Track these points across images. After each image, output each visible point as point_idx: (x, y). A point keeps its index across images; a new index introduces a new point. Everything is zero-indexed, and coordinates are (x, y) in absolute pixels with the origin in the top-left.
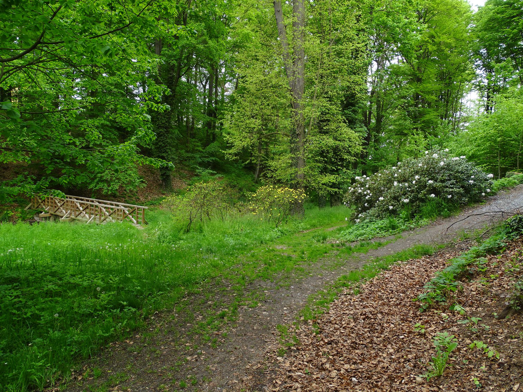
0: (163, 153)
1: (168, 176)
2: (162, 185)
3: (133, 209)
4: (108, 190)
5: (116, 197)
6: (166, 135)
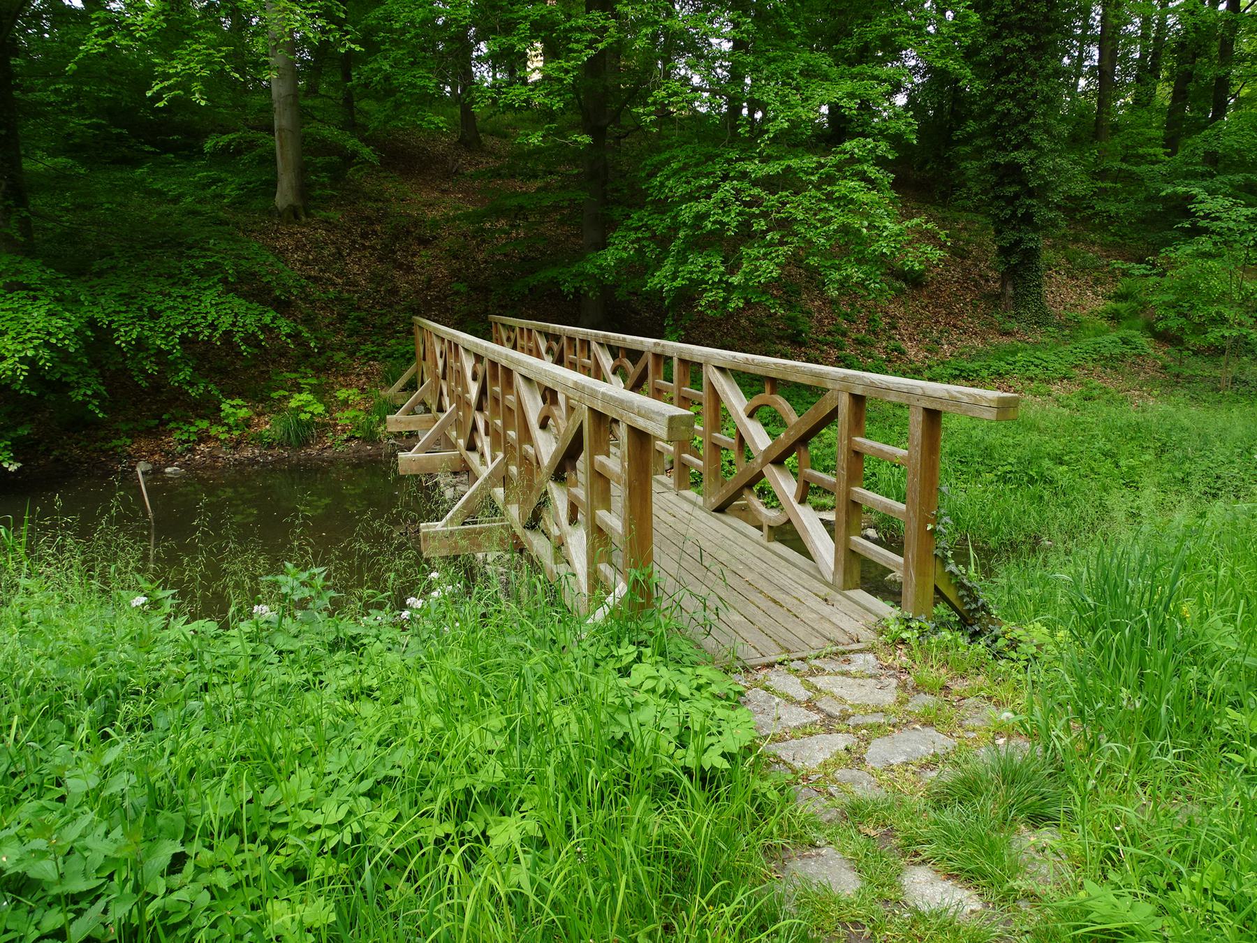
0: (1017, 147)
1: (1031, 255)
2: (998, 297)
3: (815, 413)
4: (730, 288)
5: (802, 344)
6: (1034, 64)
